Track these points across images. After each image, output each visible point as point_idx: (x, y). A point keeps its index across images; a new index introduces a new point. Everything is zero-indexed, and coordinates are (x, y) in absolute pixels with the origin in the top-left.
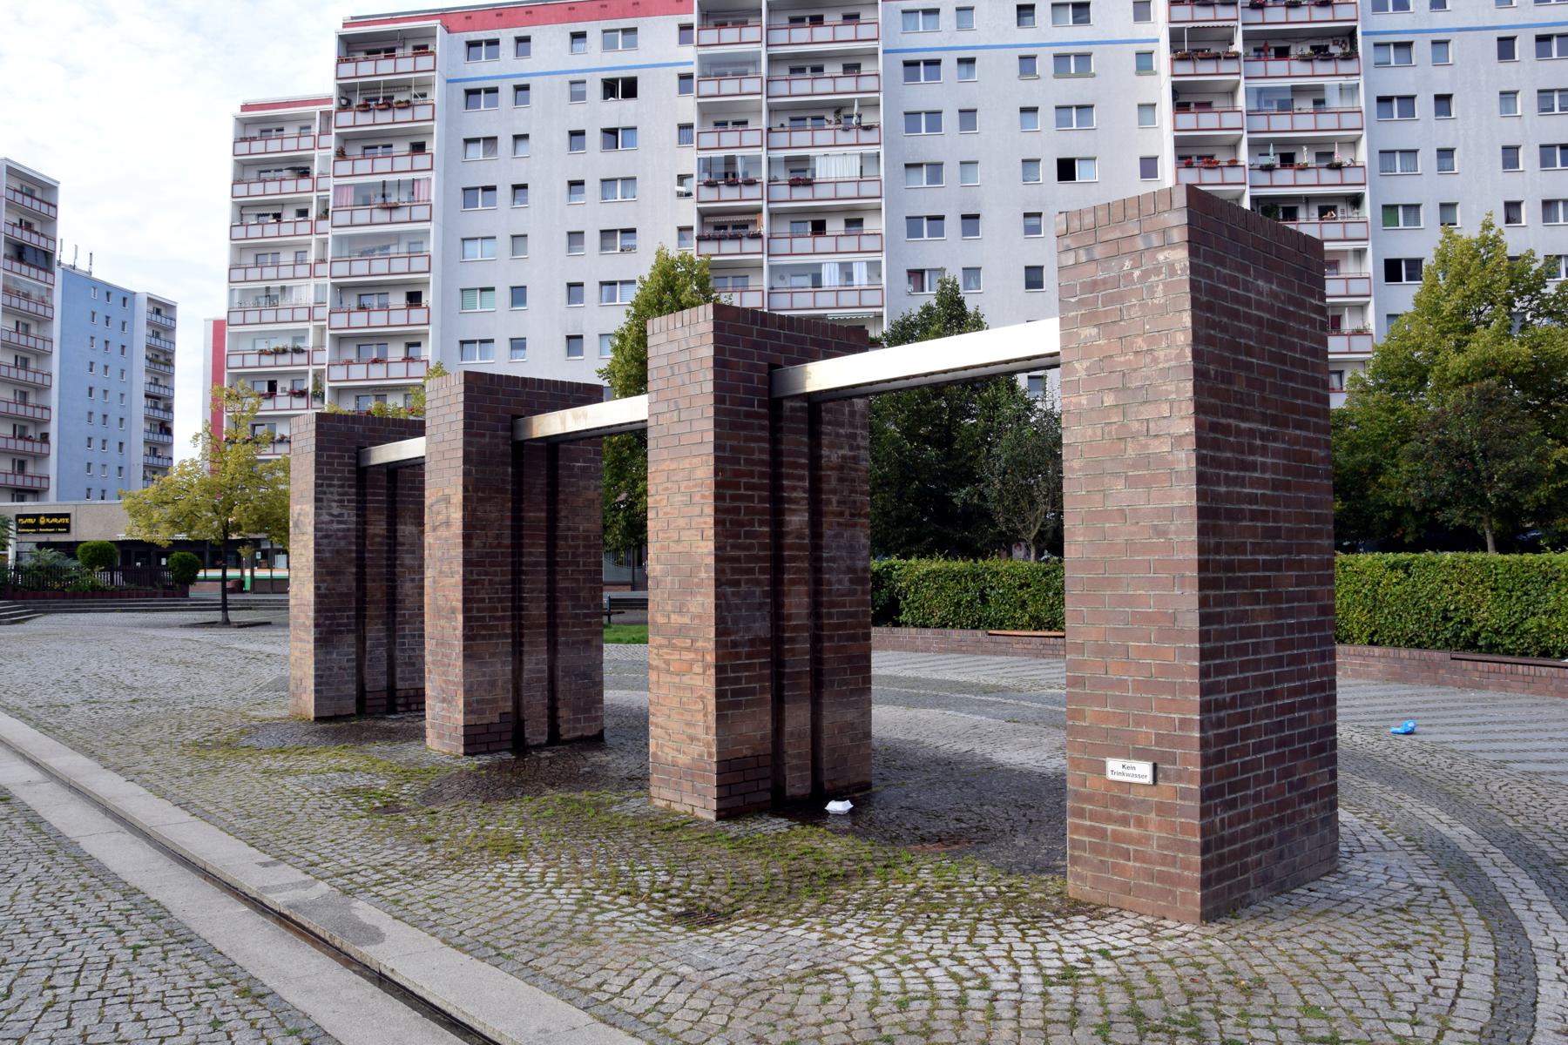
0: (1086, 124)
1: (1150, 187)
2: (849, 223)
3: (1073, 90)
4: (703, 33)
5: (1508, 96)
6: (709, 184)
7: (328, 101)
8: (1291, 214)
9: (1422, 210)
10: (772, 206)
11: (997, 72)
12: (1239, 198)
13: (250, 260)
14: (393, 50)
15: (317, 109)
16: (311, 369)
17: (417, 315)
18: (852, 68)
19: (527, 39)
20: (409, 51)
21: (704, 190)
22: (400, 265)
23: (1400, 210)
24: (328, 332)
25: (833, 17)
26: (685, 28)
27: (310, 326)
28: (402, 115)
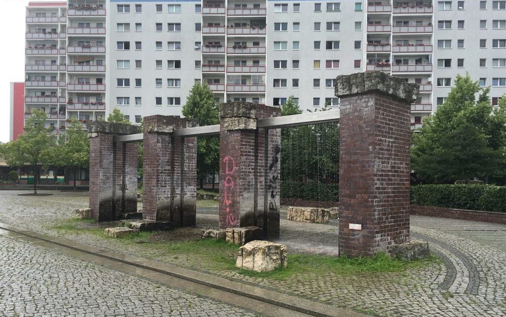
0: (337, 28)
1: (357, 71)
2: (254, 62)
3: (333, 17)
4: (204, 9)
5: (483, 22)
6: (207, 46)
7: (64, 4)
8: (407, 80)
9: (452, 41)
10: (228, 55)
11: (307, 28)
12: (389, 73)
13: (34, 63)
14: (89, 61)
15: (59, 7)
16: (59, 72)
17: (101, 87)
18: (256, 44)
19: (140, 6)
20: (95, 63)
21: (204, 48)
22: (94, 68)
23: (444, 42)
24: (67, 91)
25: (250, 6)
26: (198, 6)
27: (58, 88)
28: (93, 13)
